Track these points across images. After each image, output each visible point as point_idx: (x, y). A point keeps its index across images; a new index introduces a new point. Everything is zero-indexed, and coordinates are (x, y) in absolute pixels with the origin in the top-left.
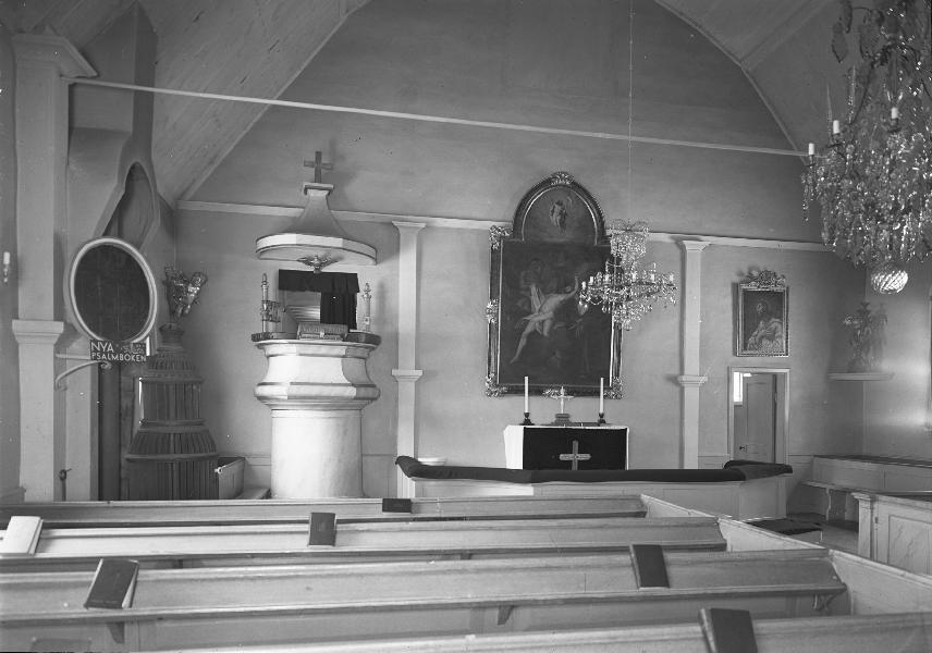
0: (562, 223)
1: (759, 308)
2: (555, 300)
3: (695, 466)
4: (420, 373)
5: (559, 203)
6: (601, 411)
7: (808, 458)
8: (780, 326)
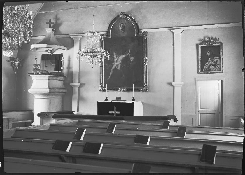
0: (124, 30)
1: (209, 53)
2: (122, 57)
3: (141, 114)
4: (80, 84)
5: (123, 23)
6: (133, 96)
7: (238, 117)
8: (219, 60)
